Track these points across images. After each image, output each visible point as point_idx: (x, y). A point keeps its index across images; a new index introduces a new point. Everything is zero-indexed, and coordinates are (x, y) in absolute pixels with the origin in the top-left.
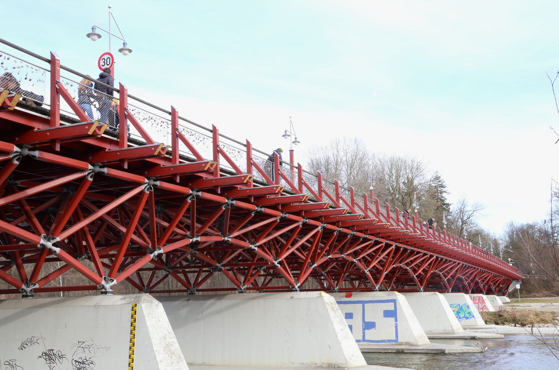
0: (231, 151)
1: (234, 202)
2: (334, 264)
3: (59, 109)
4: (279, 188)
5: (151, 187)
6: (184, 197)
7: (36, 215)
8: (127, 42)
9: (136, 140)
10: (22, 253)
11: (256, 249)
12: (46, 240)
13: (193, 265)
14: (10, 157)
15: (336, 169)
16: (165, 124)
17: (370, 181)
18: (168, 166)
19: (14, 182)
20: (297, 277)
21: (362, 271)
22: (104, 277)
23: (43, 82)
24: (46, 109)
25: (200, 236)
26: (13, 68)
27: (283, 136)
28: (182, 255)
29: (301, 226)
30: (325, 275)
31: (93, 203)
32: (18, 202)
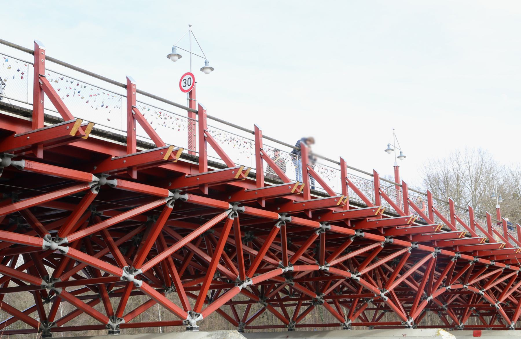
0: (323, 171)
1: (329, 227)
2: (457, 296)
3: (136, 135)
4: (379, 210)
5: (236, 213)
6: (272, 223)
7: (119, 247)
8: (208, 60)
9: (217, 163)
10: (110, 287)
11: (359, 278)
12: (128, 273)
13: (293, 297)
14: (89, 186)
15: (458, 185)
16: (249, 144)
17: (495, 198)
18: (252, 190)
19: (98, 212)
20: (409, 311)
21: (491, 305)
22: (190, 311)
23: (120, 108)
24: (122, 136)
25: (293, 265)
26: (90, 96)
27: (386, 151)
28: (279, 286)
29: (410, 253)
30: (446, 309)
31: (177, 231)
32: (101, 232)
